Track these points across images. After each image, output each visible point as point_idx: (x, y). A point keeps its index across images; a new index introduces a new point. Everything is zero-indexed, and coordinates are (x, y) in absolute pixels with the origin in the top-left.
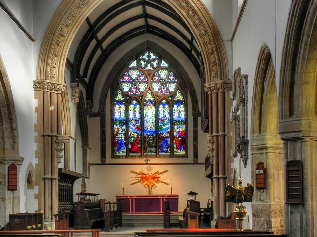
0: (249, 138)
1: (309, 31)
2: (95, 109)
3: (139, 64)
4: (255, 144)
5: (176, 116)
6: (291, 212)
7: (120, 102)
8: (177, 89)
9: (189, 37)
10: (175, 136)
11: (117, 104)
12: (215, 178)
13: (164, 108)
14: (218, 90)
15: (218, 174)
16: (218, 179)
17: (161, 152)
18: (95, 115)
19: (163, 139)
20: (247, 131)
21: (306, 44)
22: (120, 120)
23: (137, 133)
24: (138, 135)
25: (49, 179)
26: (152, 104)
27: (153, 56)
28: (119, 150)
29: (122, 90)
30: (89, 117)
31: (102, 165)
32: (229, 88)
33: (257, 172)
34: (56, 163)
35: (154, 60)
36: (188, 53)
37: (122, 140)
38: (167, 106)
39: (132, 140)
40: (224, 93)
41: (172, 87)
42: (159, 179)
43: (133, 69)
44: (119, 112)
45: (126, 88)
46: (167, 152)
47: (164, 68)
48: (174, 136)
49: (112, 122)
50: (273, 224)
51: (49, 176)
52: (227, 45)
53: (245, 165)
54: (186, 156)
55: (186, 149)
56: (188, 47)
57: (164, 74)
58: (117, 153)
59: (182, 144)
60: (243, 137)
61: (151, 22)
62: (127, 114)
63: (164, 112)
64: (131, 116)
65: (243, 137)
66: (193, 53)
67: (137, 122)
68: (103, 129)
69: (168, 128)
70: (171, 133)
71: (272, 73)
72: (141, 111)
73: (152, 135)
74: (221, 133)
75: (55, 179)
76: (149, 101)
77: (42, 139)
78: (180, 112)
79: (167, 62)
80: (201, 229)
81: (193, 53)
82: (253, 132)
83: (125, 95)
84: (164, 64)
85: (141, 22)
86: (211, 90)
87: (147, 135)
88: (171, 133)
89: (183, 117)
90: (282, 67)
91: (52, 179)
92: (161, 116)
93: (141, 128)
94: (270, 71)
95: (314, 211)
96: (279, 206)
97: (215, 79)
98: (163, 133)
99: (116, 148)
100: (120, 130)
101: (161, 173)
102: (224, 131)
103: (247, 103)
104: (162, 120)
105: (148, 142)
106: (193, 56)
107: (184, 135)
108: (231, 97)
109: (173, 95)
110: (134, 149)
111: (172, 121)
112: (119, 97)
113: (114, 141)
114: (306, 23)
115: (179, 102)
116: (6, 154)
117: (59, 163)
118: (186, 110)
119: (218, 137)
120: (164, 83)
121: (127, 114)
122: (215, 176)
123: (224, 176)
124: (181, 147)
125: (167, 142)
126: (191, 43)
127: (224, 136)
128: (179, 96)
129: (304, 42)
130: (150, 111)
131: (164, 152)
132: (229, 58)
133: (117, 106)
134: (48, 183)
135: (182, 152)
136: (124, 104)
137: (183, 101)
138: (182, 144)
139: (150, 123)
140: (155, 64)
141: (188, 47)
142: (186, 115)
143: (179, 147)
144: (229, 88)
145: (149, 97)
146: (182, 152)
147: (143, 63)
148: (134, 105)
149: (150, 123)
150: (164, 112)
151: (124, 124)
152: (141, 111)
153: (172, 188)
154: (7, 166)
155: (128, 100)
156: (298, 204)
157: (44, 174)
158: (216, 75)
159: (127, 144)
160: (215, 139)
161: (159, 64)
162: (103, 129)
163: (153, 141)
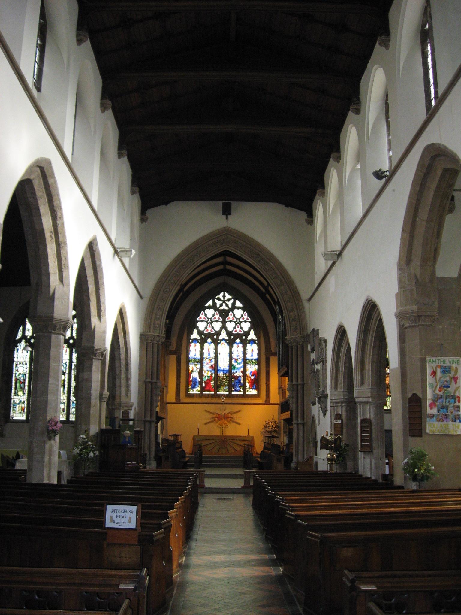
0: (328, 392)
1: (374, 328)
2: (173, 348)
3: (215, 304)
4: (333, 398)
5: (248, 357)
6: (364, 458)
7: (195, 340)
8: (250, 329)
9: (266, 284)
10: (248, 375)
11: (192, 342)
12: (295, 423)
13: (238, 346)
14: (297, 343)
15: (298, 420)
16: (298, 424)
17: (233, 391)
18: (172, 353)
19: (237, 378)
20: (326, 387)
21: (372, 336)
22: (195, 359)
23: (211, 372)
24: (212, 373)
25: (148, 421)
26: (226, 342)
27: (228, 297)
28: (193, 388)
29: (197, 328)
30: (167, 356)
31: (178, 404)
32: (307, 341)
33: (335, 421)
34: (154, 407)
35: (229, 300)
36: (262, 296)
37: (196, 379)
38: (240, 345)
39: (205, 379)
40: (303, 346)
41: (246, 326)
42: (213, 416)
43: (209, 307)
44: (194, 350)
45: (201, 326)
46: (240, 391)
47: (238, 308)
48: (246, 375)
49: (187, 359)
50: (348, 466)
51: (149, 419)
52: (306, 304)
53: (325, 414)
54: (257, 396)
55: (258, 389)
56: (264, 291)
57: (238, 313)
58: (191, 392)
59: (254, 383)
60: (323, 392)
61: (229, 267)
62: (202, 353)
63: (238, 349)
64: (206, 355)
65: (323, 392)
66: (267, 296)
67: (211, 360)
68: (179, 368)
69: (241, 367)
70: (244, 372)
71: (347, 343)
72: (216, 349)
73: (225, 374)
74: (300, 382)
75: (153, 421)
76: (224, 339)
77: (144, 386)
78: (253, 351)
79: (241, 302)
80: (285, 471)
81: (267, 296)
82: (331, 387)
83: (200, 333)
84: (238, 304)
85: (220, 267)
86: (291, 342)
87: (221, 374)
88: (244, 372)
89: (255, 357)
90: (356, 349)
91: (150, 422)
92: (234, 356)
93: (215, 368)
94: (344, 344)
95: (337, 398)
96: (23, 351)
97: (295, 333)
98: (236, 372)
99: (190, 387)
100: (195, 369)
101: (234, 413)
102: (303, 381)
103: (326, 363)
104: (235, 359)
105: (221, 381)
106: (267, 298)
107: (257, 374)
108: (309, 349)
109: (247, 334)
110: (208, 388)
111: (245, 360)
112: (195, 335)
113: (188, 380)
114: (371, 324)
115: (252, 341)
116: (122, 401)
117: (157, 406)
118: (259, 350)
119: (297, 385)
120: (238, 323)
121: (202, 353)
122: (294, 421)
123: (303, 422)
124: (253, 386)
125: (240, 381)
126: (266, 288)
127: (303, 385)
128: (252, 336)
129: (371, 335)
130: (223, 348)
131: (237, 391)
132: (308, 319)
133: (193, 345)
134: (147, 424)
135: (254, 392)
136: (198, 342)
137: (256, 340)
138: (254, 383)
139: (223, 364)
140: (230, 303)
141: (264, 291)
142: (259, 354)
143: (251, 387)
144: (307, 341)
145: (224, 335)
146: (254, 392)
147: (218, 303)
148: (209, 343)
149: (223, 364)
150: (238, 349)
151: (199, 362)
152: (216, 349)
153: (249, 430)
154: (122, 411)
155: (204, 338)
156: (370, 451)
157: (145, 417)
158: (295, 330)
159: (201, 383)
160: (295, 387)
161: (234, 304)
162: (179, 368)
163: (227, 380)
